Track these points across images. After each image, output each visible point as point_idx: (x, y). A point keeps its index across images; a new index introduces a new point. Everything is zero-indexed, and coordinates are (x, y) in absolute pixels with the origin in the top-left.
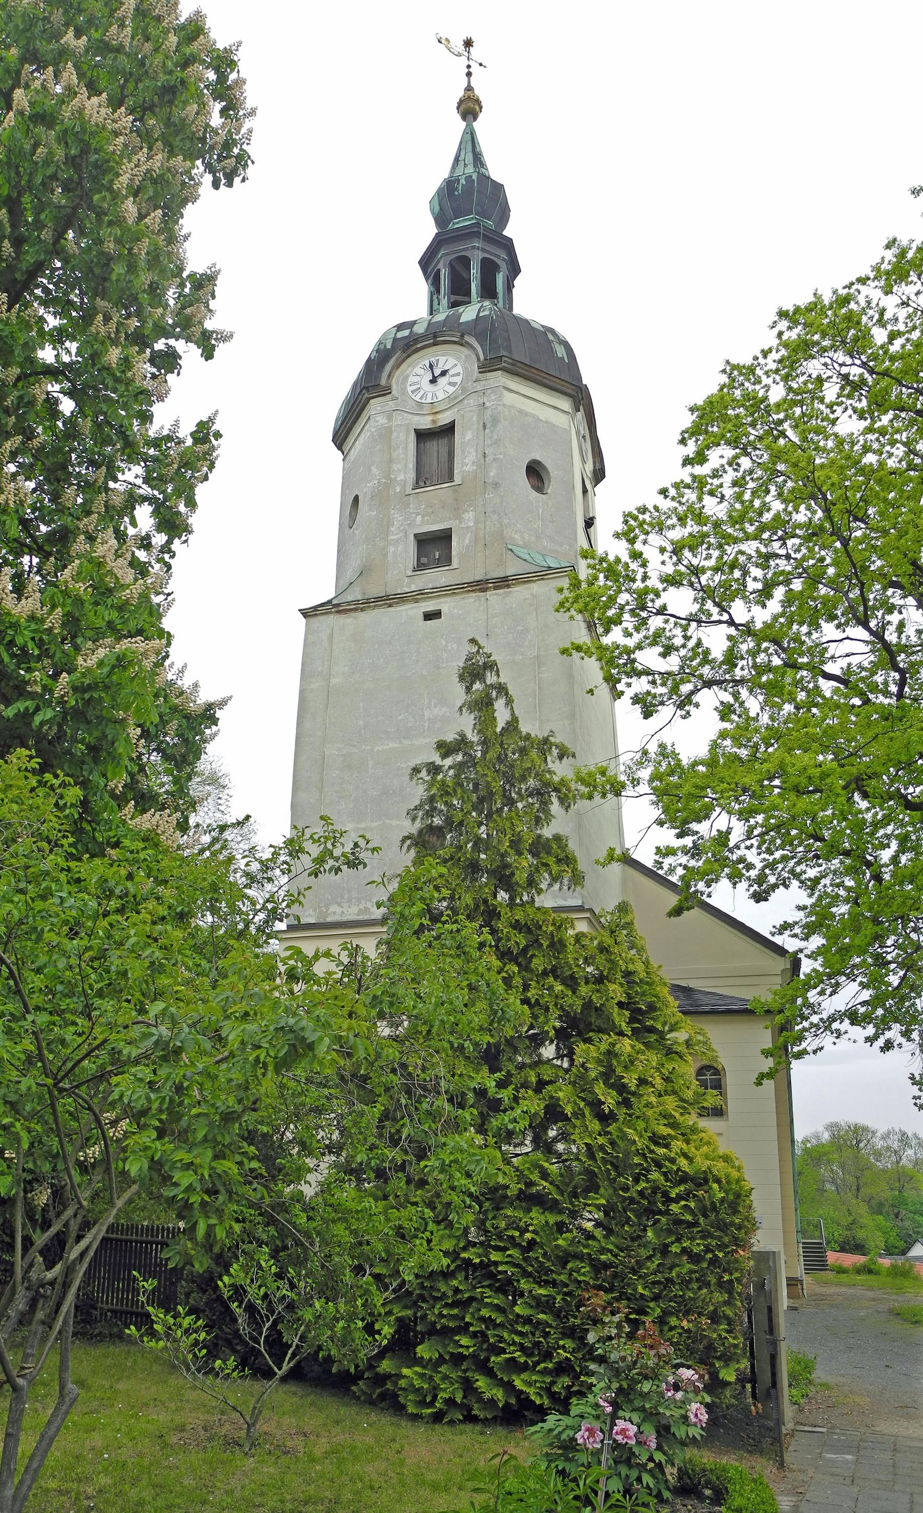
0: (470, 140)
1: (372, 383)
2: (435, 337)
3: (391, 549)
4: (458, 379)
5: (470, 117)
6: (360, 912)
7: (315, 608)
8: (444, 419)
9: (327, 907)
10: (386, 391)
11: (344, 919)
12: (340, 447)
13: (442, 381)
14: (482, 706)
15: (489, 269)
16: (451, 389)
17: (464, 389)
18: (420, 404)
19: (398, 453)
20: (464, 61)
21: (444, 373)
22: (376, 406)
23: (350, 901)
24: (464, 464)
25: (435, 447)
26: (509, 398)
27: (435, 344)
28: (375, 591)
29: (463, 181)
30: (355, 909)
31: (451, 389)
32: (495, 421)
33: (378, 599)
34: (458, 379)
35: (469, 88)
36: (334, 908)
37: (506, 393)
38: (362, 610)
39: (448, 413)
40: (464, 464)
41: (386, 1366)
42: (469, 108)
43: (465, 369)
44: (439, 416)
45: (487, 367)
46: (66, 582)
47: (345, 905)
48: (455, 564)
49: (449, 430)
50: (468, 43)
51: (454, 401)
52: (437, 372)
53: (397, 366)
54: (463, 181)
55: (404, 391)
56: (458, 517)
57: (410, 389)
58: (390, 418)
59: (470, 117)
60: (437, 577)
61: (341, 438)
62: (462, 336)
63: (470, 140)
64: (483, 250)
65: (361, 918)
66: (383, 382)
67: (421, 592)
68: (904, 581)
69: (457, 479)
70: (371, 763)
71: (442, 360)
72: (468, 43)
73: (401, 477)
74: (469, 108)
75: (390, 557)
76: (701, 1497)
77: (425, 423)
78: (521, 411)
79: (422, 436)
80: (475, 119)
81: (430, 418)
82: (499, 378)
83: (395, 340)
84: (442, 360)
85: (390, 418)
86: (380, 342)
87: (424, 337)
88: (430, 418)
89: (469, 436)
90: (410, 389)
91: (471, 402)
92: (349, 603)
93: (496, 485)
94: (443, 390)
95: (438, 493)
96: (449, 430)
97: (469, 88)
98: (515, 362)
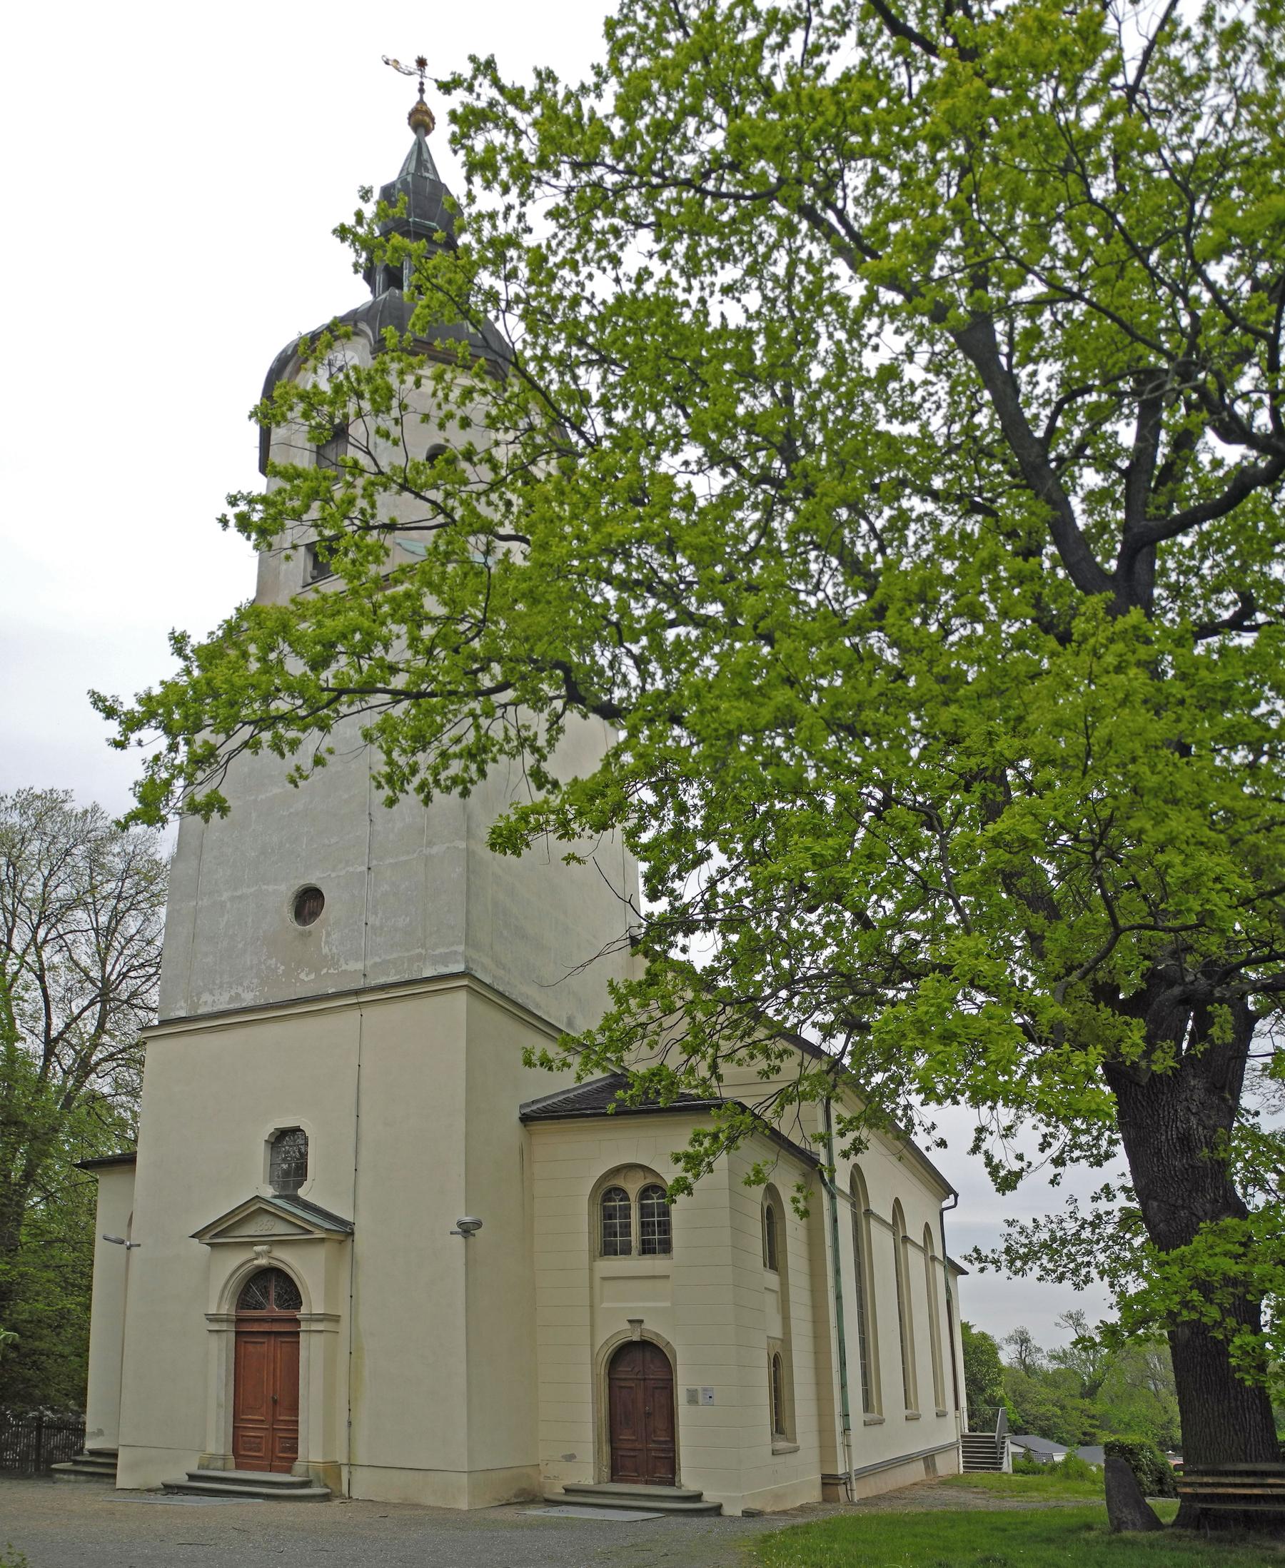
6: (231, 1000)
9: (199, 995)
11: (215, 1009)
14: (110, 713)
20: (416, 79)
23: (221, 987)
30: (226, 997)
35: (421, 102)
36: (206, 997)
46: (227, 681)
47: (217, 992)
50: (422, 63)
59: (422, 131)
62: (355, 325)
65: (232, 1006)
68: (819, 475)
70: (254, 815)
72: (422, 63)
75: (282, 577)
97: (421, 102)
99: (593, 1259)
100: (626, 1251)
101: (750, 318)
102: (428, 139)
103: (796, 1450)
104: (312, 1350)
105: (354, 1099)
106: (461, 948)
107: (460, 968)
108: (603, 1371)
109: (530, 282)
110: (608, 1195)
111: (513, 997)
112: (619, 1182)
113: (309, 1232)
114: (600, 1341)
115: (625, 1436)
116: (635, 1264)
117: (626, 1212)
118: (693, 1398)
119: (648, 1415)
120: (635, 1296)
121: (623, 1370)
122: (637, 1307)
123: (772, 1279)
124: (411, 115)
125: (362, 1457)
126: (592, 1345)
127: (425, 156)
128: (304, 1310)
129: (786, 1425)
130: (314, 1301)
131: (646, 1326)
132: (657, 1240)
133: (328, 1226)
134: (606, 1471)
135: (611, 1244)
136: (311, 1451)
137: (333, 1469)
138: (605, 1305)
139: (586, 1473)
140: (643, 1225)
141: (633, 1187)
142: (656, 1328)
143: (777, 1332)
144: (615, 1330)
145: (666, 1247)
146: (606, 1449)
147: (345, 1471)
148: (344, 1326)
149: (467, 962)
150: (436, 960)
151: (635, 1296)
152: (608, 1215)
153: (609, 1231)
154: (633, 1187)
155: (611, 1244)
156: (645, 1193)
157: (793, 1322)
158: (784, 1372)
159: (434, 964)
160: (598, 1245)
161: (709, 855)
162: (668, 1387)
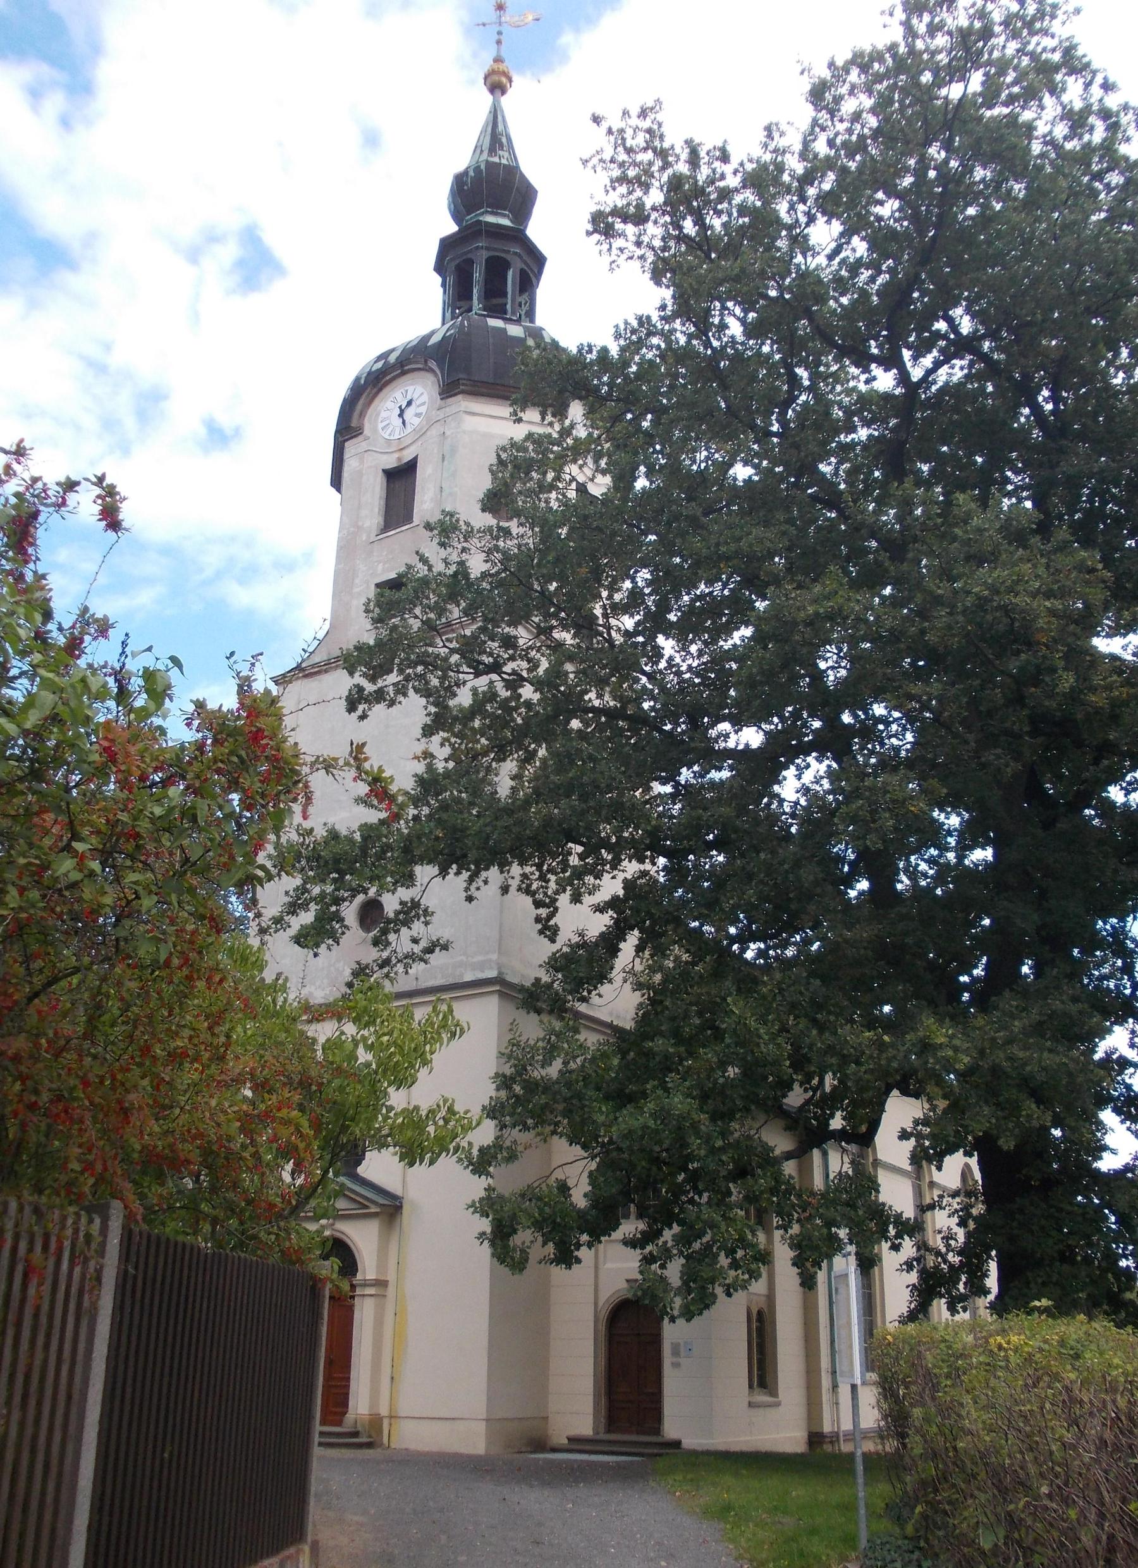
0: (495, 115)
1: (348, 427)
2: (402, 366)
5: (498, 92)
8: (408, 456)
12: (339, 490)
15: (497, 268)
18: (388, 442)
22: (352, 448)
27: (404, 373)
34: (423, 409)
35: (496, 136)
37: (468, 418)
38: (326, 671)
41: (10, 888)
45: (448, 390)
51: (421, 434)
55: (375, 430)
58: (362, 461)
61: (337, 481)
63: (495, 115)
64: (487, 249)
66: (354, 424)
73: (367, 524)
76: (102, 1267)
77: (391, 462)
80: (503, 92)
81: (396, 455)
82: (463, 403)
83: (369, 373)
85: (362, 461)
87: (393, 367)
88: (396, 455)
91: (434, 432)
92: (313, 666)
97: (496, 136)
98: (475, 383)
102: (505, 101)
103: (778, 1404)
104: (365, 1313)
105: (440, 1423)
106: (494, 957)
107: (492, 974)
108: (602, 1328)
113: (367, 1207)
114: (602, 1301)
118: (676, 1352)
125: (404, 1409)
126: (596, 1304)
127: (501, 127)
128: (359, 1276)
130: (368, 1269)
133: (381, 1201)
136: (360, 1405)
137: (376, 1422)
138: (609, 1265)
147: (386, 1423)
148: (391, 1290)
149: (499, 968)
150: (473, 967)
159: (473, 970)
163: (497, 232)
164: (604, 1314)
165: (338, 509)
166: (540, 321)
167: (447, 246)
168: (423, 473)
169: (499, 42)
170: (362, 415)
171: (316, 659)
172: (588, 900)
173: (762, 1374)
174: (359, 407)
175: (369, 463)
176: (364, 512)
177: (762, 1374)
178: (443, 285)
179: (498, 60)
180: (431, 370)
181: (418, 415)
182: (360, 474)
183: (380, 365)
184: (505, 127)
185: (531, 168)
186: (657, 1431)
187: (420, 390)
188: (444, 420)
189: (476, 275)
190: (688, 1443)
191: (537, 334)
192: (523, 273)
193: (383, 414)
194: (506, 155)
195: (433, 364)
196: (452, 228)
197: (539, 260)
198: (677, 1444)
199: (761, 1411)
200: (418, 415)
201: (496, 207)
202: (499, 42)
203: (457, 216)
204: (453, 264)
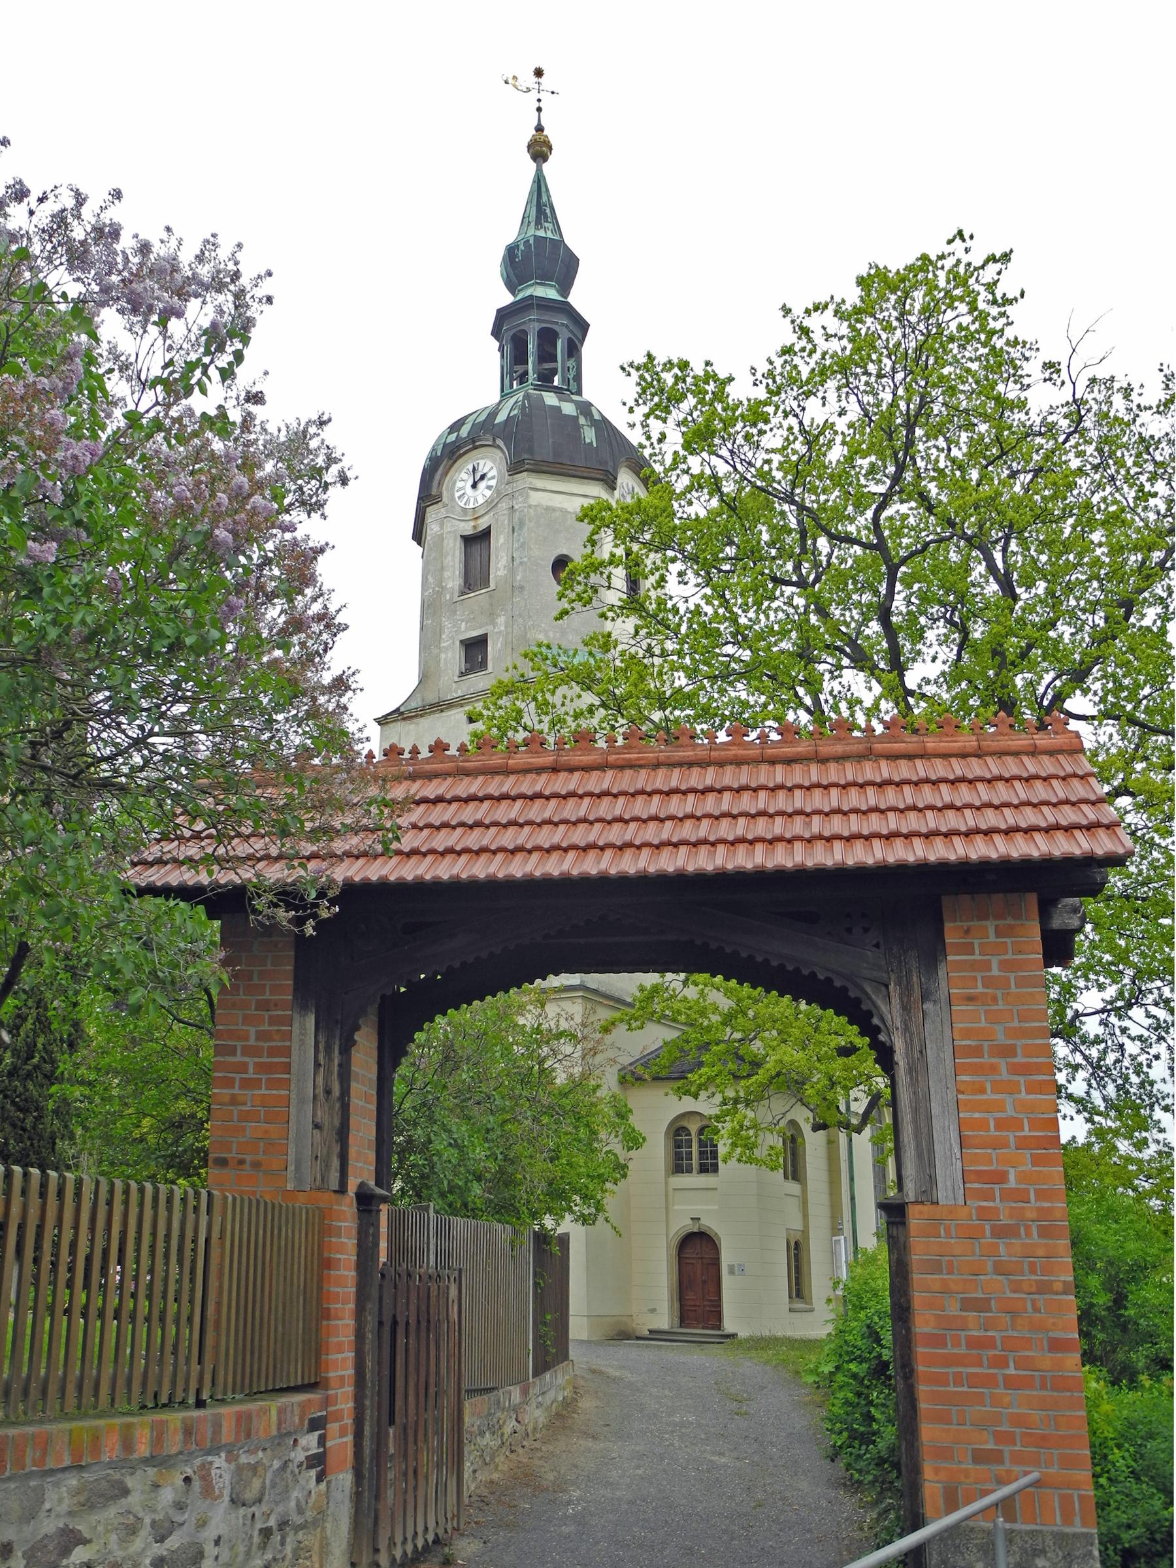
0: (539, 183)
1: (429, 494)
3: (443, 656)
4: (493, 483)
7: (385, 717)
8: (483, 524)
10: (437, 499)
13: (482, 485)
15: (547, 337)
16: (488, 493)
17: (498, 492)
18: (464, 510)
19: (448, 561)
20: (534, 95)
21: (483, 477)
22: (432, 514)
24: (497, 569)
25: (476, 549)
26: (536, 498)
27: (475, 448)
28: (432, 698)
29: (522, 247)
31: (488, 493)
32: (522, 523)
33: (432, 706)
34: (493, 483)
37: (532, 493)
39: (486, 518)
40: (497, 569)
42: (540, 150)
43: (499, 472)
44: (480, 521)
45: (515, 467)
48: (490, 670)
49: (486, 534)
51: (491, 505)
52: (478, 477)
53: (446, 473)
54: (522, 247)
56: (494, 624)
57: (457, 495)
58: (442, 526)
60: (480, 681)
61: (418, 535)
63: (539, 183)
64: (538, 321)
66: (434, 492)
67: (463, 698)
69: (492, 586)
71: (482, 462)
73: (450, 585)
74: (540, 150)
77: (468, 529)
78: (548, 509)
79: (468, 540)
80: (545, 159)
81: (472, 523)
82: (526, 480)
83: (445, 445)
84: (482, 462)
85: (442, 526)
86: (433, 449)
87: (465, 443)
88: (472, 523)
89: (501, 541)
90: (457, 495)
92: (410, 711)
93: (522, 588)
94: (483, 493)
95: (479, 597)
96: (486, 534)
98: (537, 463)
99: (667, 1176)
100: (690, 1171)
101: (1077, 1015)
102: (545, 166)
103: (812, 1310)
108: (674, 1252)
109: (851, 425)
110: (677, 1132)
111: (617, 995)
112: (685, 1124)
115: (690, 1296)
116: (695, 1180)
117: (689, 1143)
118: (731, 1271)
119: (705, 1282)
120: (697, 1202)
121: (689, 1252)
122: (696, 1209)
123: (794, 1187)
124: (529, 147)
129: (805, 1292)
131: (702, 1222)
132: (709, 1165)
134: (677, 1320)
135: (679, 1166)
139: (663, 1320)
140: (701, 1153)
141: (694, 1128)
142: (710, 1223)
143: (798, 1225)
144: (681, 1224)
145: (715, 1169)
146: (677, 1305)
151: (697, 1202)
152: (678, 1145)
153: (678, 1157)
154: (694, 1128)
155: (679, 1166)
156: (701, 1131)
157: (811, 1218)
158: (803, 1254)
160: (671, 1166)
161: (219, 1416)
162: (716, 1262)
163: (545, 305)
164: (675, 1243)
165: (418, 563)
166: (588, 394)
167: (503, 315)
168: (498, 541)
169: (539, 110)
170: (440, 484)
171: (413, 705)
172: (1169, 1018)
173: (798, 1289)
174: (437, 476)
175: (448, 529)
176: (447, 574)
177: (798, 1289)
178: (501, 349)
179: (539, 129)
180: (499, 447)
181: (489, 488)
182: (441, 538)
183: (453, 437)
184: (549, 196)
185: (573, 240)
186: (719, 1328)
187: (491, 463)
188: (512, 496)
189: (530, 346)
190: (743, 1334)
191: (586, 408)
192: (570, 341)
193: (459, 484)
194: (550, 226)
195: (500, 442)
196: (507, 299)
197: (583, 326)
198: (734, 1336)
199: (798, 1315)
200: (489, 488)
201: (544, 278)
202: (539, 110)
203: (512, 287)
204: (511, 333)
